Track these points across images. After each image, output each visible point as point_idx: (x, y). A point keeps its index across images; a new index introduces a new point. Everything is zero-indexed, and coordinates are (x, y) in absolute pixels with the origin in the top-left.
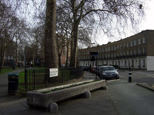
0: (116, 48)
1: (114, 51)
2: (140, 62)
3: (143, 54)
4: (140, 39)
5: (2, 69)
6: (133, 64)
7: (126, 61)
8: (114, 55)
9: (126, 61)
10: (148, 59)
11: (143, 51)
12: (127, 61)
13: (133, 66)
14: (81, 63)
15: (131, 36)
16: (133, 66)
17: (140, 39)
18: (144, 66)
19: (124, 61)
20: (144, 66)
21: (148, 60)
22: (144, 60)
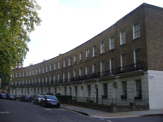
0: (71, 62)
1: (67, 67)
2: (77, 89)
3: (122, 69)
4: (104, 44)
5: (98, 82)
6: (106, 92)
7: (89, 87)
8: (67, 76)
9: (89, 87)
10: (152, 77)
11: (135, 59)
12: (93, 86)
13: (105, 97)
14: (17, 90)
15: (45, 62)
16: (105, 97)
17: (125, 33)
18: (139, 97)
19: (101, 85)
20: (139, 97)
21: (150, 80)
22: (139, 82)
